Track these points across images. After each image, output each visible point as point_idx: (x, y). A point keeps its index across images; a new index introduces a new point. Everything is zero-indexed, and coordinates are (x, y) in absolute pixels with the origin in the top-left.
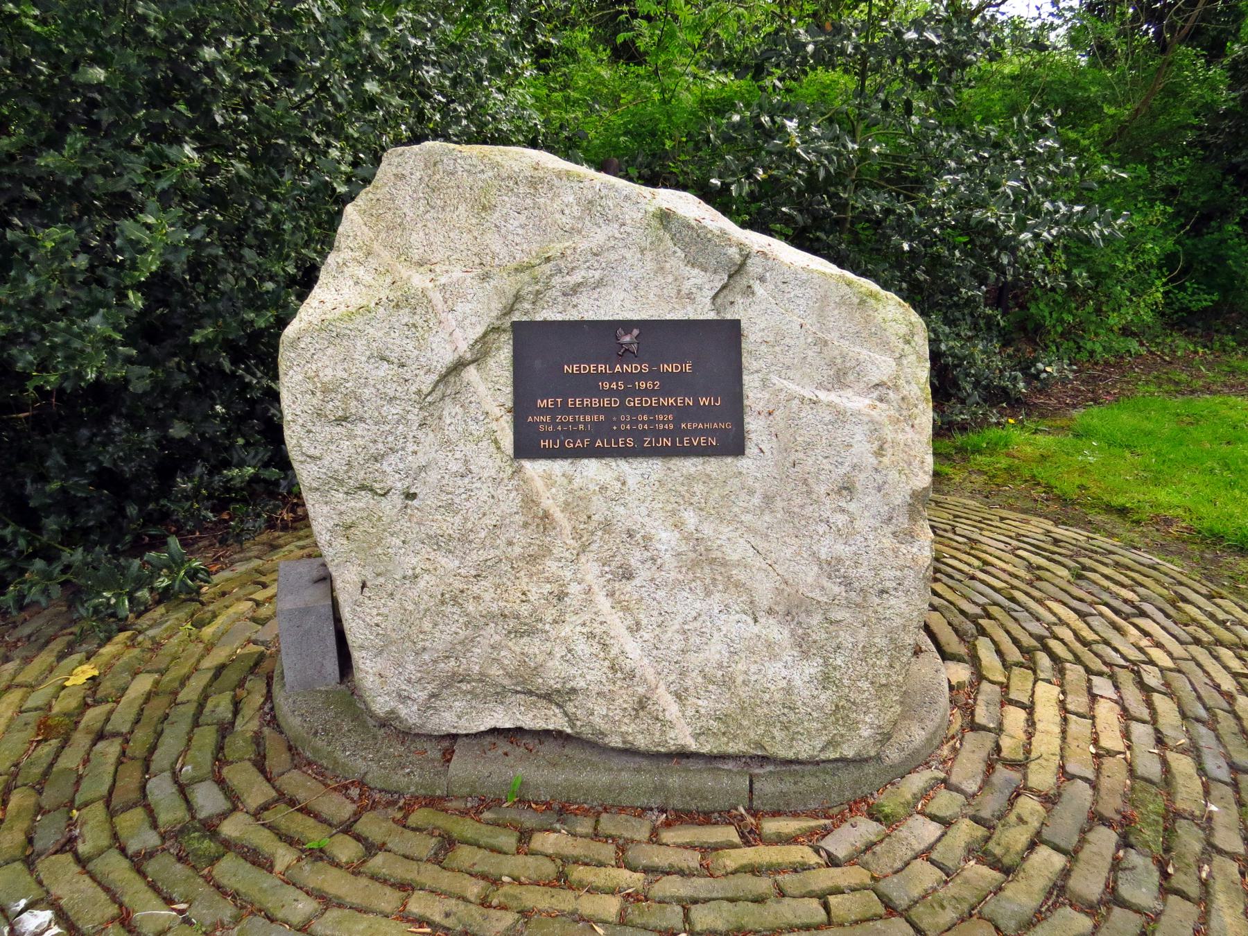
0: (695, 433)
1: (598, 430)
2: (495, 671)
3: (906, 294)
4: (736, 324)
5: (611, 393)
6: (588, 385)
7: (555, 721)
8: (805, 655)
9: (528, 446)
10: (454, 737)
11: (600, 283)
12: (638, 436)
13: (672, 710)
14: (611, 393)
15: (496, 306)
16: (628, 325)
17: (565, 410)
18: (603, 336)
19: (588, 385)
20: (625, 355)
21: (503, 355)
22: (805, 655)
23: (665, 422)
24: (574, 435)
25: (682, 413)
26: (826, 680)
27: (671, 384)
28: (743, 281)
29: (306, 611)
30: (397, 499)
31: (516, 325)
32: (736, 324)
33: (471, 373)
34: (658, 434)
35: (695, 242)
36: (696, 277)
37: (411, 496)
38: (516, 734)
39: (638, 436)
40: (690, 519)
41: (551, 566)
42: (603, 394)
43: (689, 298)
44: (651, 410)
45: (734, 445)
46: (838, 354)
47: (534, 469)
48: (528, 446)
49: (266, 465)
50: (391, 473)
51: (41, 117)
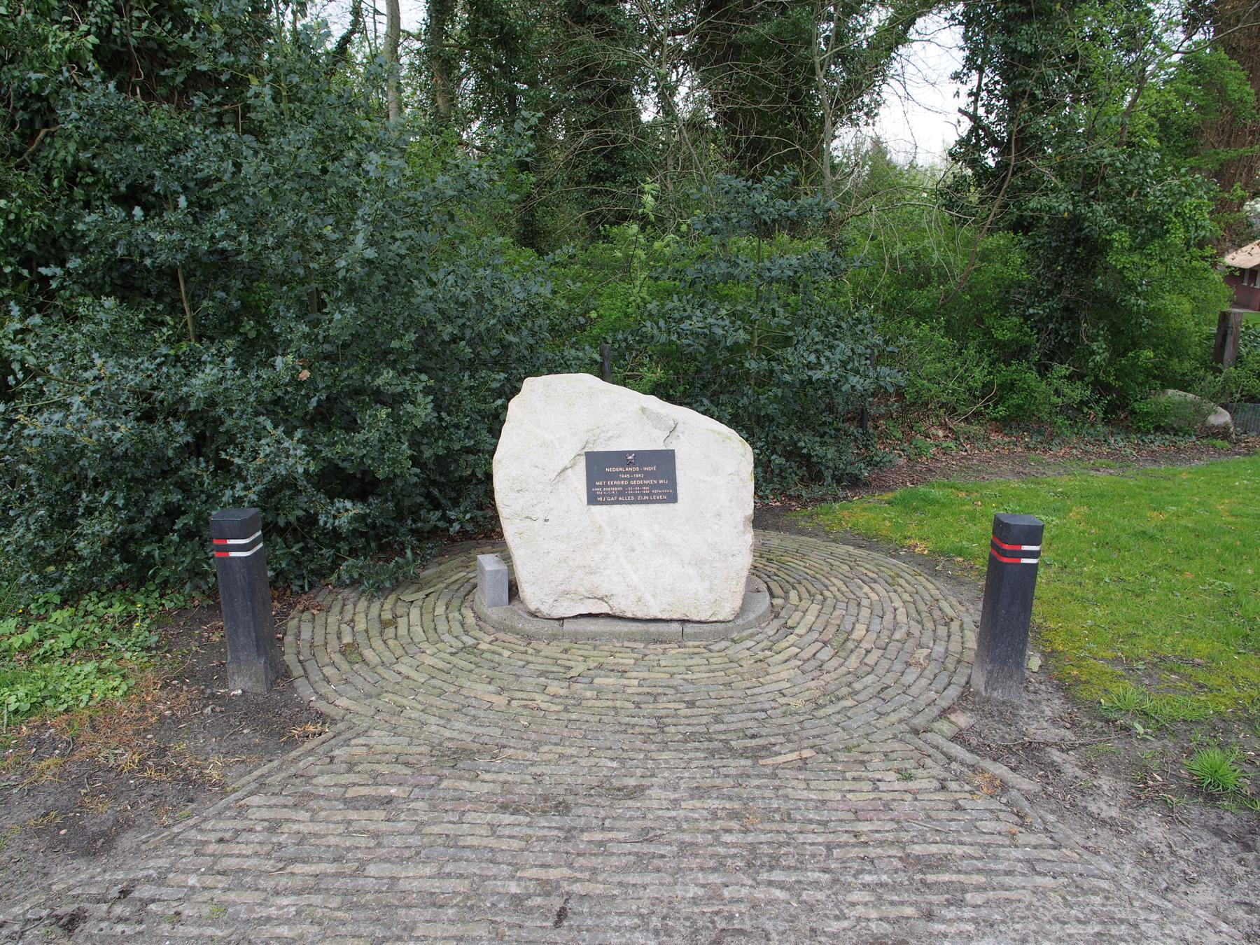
0: (658, 494)
1: (620, 494)
2: (580, 589)
3: (476, 493)
4: (673, 451)
5: (624, 479)
6: (615, 476)
7: (604, 609)
8: (703, 580)
9: (593, 500)
10: (563, 619)
11: (619, 436)
12: (636, 495)
13: (652, 602)
14: (624, 479)
15: (580, 446)
16: (630, 453)
17: (607, 486)
18: (620, 458)
19: (615, 476)
20: (630, 464)
21: (582, 463)
22: (703, 580)
23: (646, 490)
24: (611, 495)
25: (653, 487)
26: (711, 590)
27: (648, 475)
28: (675, 434)
29: (497, 572)
30: (541, 522)
31: (587, 453)
32: (673, 451)
33: (569, 472)
34: (643, 495)
35: (656, 419)
36: (657, 432)
37: (546, 520)
38: (590, 615)
39: (636, 495)
40: (657, 528)
41: (602, 547)
42: (622, 479)
43: (653, 442)
44: (640, 486)
45: (673, 498)
46: (715, 459)
47: (596, 509)
48: (593, 500)
49: (439, 520)
50: (539, 513)
51: (1199, 405)
